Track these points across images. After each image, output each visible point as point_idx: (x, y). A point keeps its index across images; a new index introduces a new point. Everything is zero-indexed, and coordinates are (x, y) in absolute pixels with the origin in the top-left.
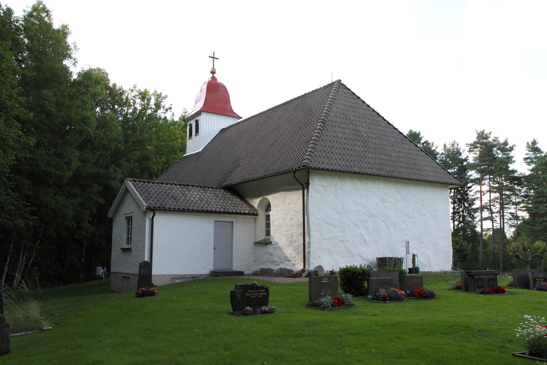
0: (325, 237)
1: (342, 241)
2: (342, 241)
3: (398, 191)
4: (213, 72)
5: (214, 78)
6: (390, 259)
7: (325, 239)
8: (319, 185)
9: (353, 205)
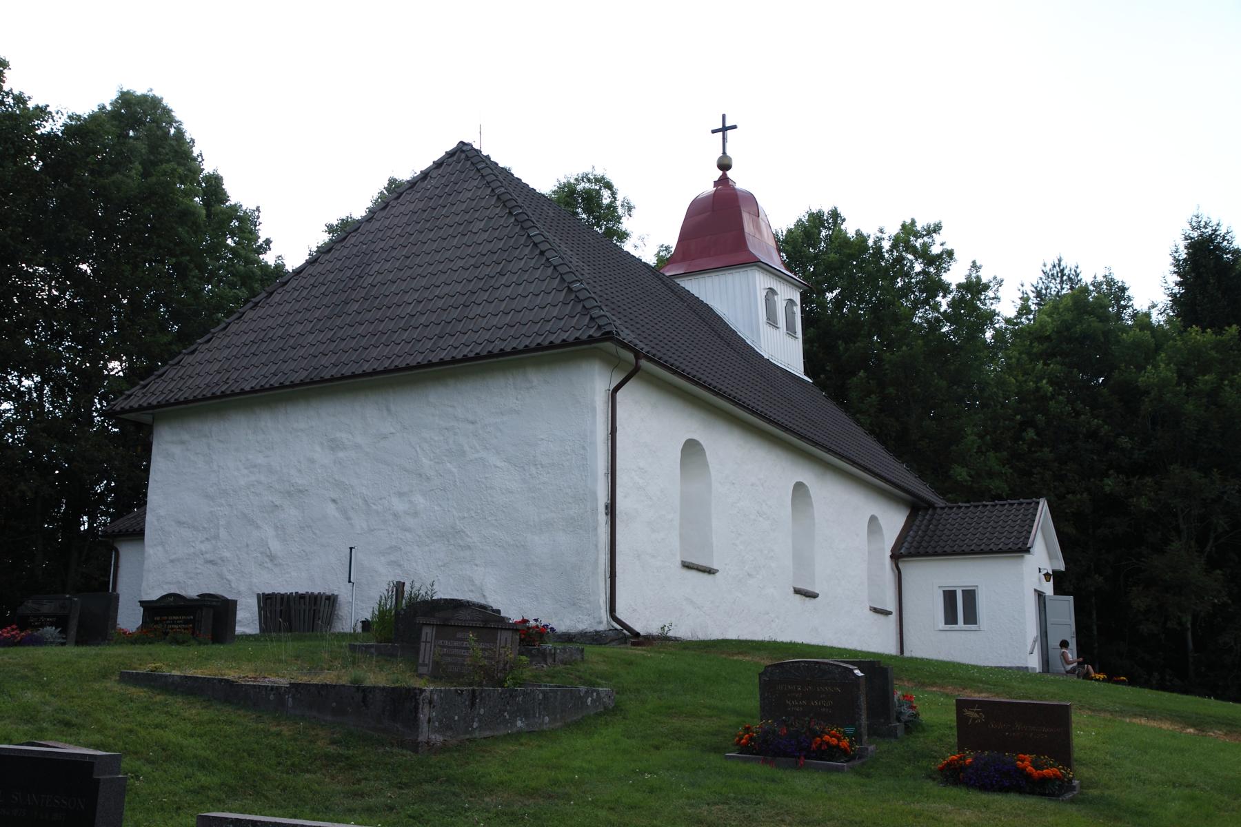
0: (173, 557)
1: (211, 562)
2: (211, 562)
3: (389, 410)
4: (724, 165)
5: (723, 181)
6: (302, 597)
7: (172, 561)
8: (172, 442)
9: (246, 472)
